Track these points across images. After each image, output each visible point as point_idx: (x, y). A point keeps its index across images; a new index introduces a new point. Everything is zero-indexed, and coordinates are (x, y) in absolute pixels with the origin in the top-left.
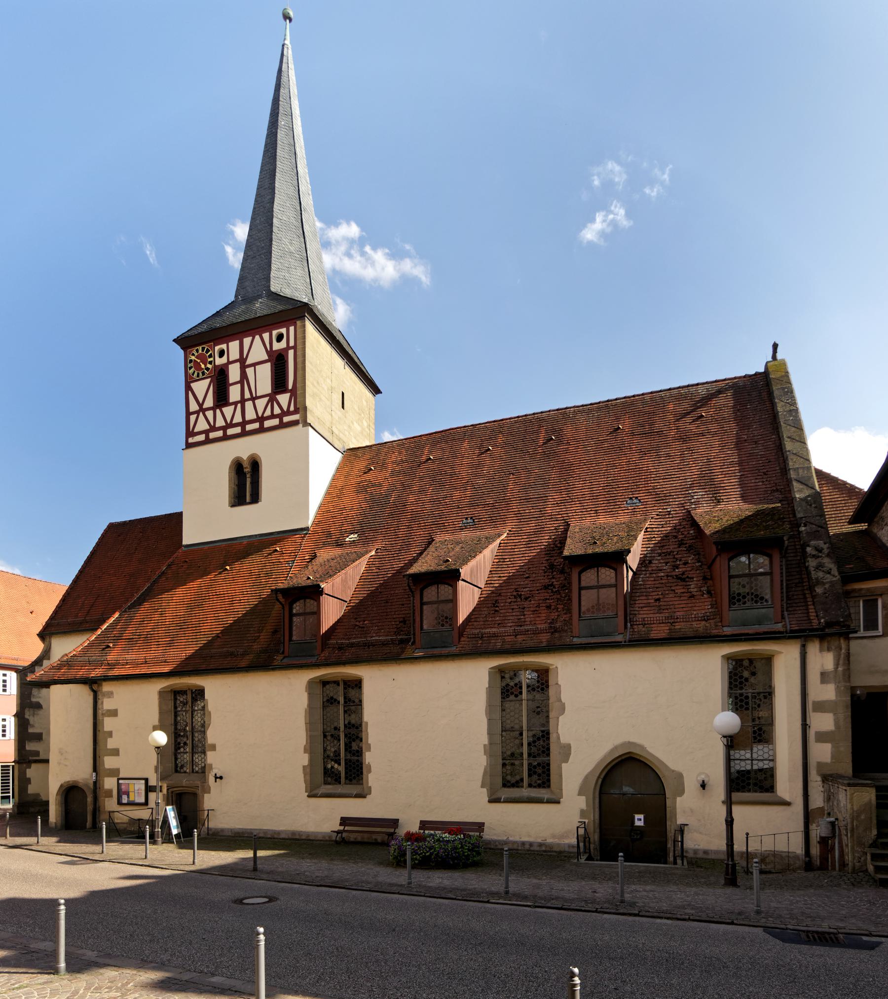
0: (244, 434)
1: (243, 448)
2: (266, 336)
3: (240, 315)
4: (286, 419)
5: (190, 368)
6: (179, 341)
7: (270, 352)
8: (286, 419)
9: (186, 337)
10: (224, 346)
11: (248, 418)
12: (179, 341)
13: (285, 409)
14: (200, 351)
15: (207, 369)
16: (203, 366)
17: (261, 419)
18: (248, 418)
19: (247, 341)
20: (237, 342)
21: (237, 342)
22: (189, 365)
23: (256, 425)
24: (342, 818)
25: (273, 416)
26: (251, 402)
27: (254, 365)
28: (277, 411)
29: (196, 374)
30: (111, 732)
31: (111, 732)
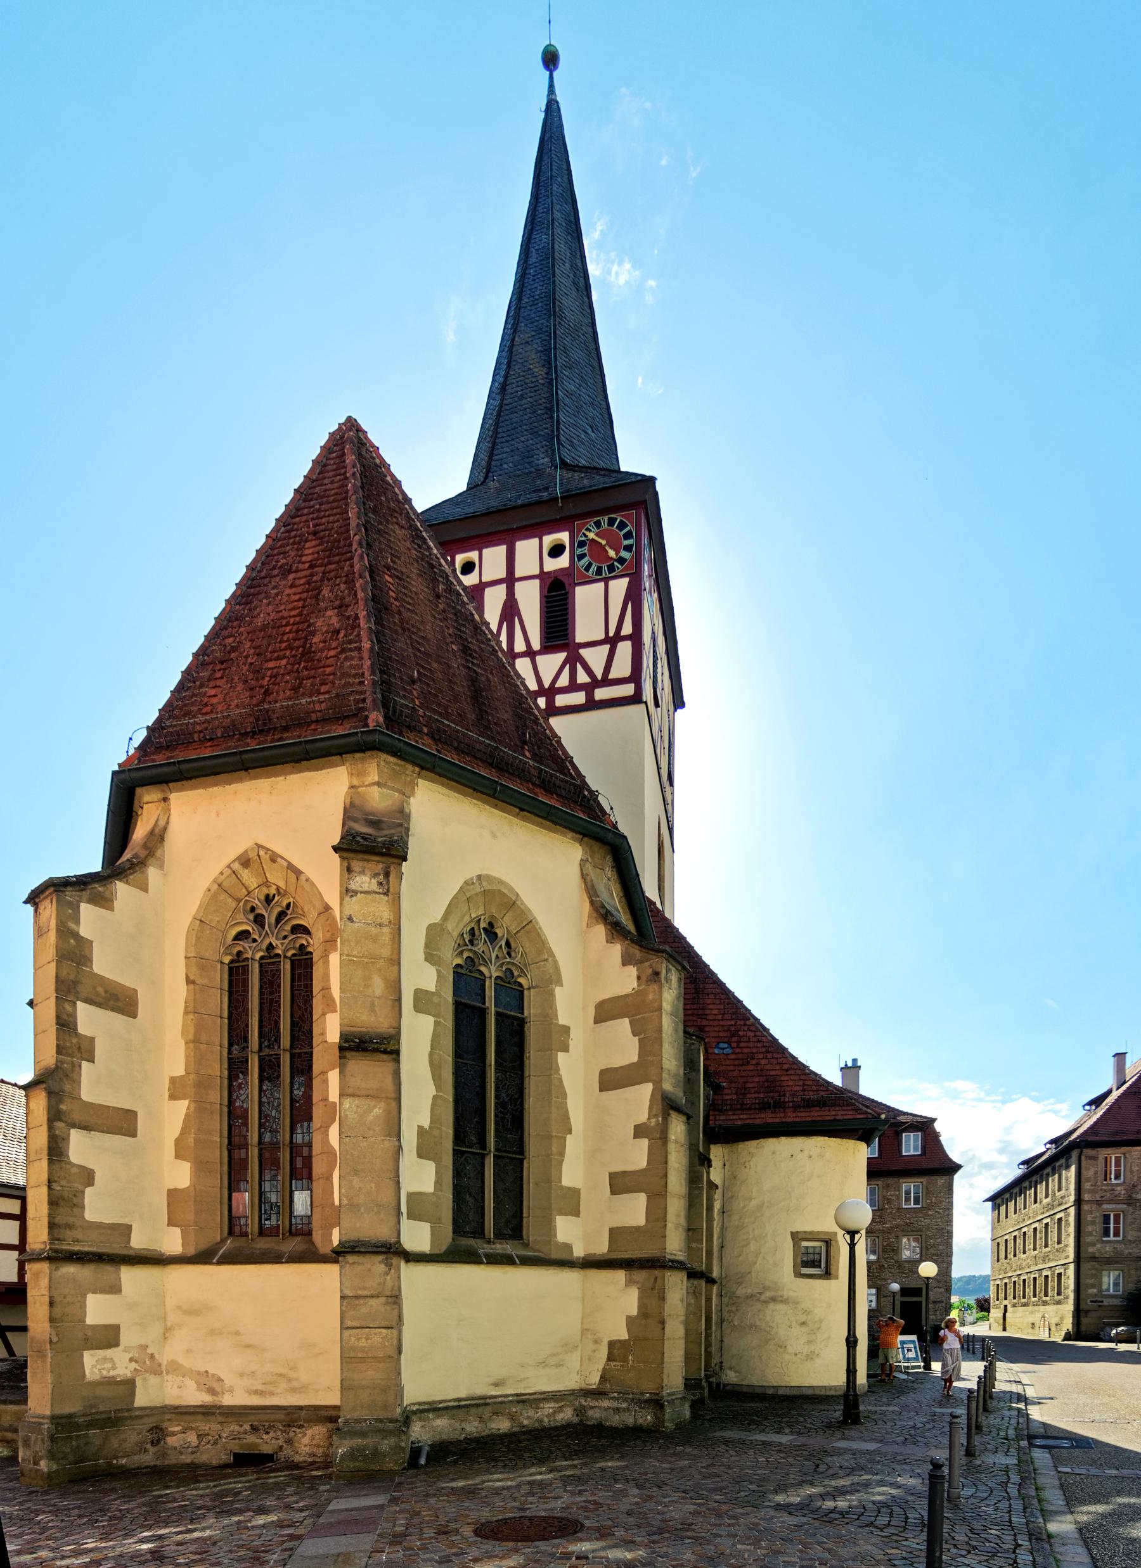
4: (600, 694)
5: (581, 557)
8: (600, 694)
10: (473, 555)
13: (599, 675)
14: (605, 525)
15: (621, 560)
16: (612, 553)
19: (521, 546)
20: (502, 549)
21: (502, 549)
24: (613, 1176)
25: (573, 687)
28: (582, 677)
29: (594, 568)
30: (637, 1135)
31: (637, 1135)
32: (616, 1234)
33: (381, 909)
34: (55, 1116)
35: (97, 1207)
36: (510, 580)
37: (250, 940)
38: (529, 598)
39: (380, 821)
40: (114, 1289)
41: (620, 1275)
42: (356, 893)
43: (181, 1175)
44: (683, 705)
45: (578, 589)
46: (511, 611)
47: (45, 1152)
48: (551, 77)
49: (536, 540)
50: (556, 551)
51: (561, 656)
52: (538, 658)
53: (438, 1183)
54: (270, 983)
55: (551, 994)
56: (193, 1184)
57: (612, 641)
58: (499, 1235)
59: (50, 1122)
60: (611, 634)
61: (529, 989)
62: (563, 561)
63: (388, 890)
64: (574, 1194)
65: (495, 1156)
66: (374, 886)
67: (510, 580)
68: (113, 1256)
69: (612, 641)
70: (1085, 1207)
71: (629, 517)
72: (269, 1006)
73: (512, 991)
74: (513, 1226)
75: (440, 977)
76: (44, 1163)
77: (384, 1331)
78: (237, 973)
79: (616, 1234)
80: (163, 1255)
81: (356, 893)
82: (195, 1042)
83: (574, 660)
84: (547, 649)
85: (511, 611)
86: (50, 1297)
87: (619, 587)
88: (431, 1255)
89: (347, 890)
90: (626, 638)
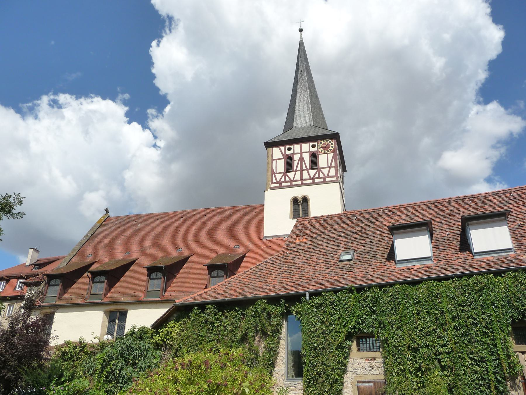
0: (292, 186)
1: (299, 192)
2: (282, 148)
4: (327, 179)
6: (265, 143)
10: (292, 147)
17: (313, 179)
23: (311, 181)
25: (319, 178)
38: (307, 157)
48: (301, 35)
50: (314, 146)
57: (329, 167)
62: (315, 149)
67: (301, 153)
69: (329, 167)
70: (219, 275)
83: (319, 170)
85: (302, 159)
90: (333, 167)
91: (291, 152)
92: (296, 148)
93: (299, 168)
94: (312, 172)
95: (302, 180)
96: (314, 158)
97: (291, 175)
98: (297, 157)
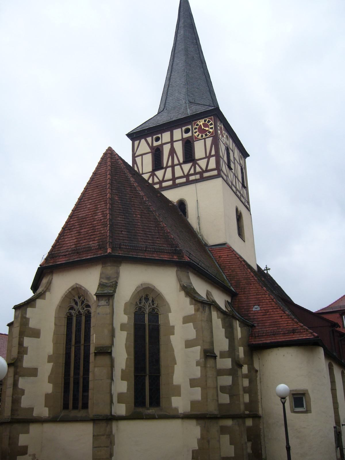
2: (149, 139)
3: (165, 119)
4: (206, 175)
5: (195, 133)
6: (129, 135)
7: (151, 147)
8: (206, 175)
9: (129, 134)
10: (160, 136)
11: (177, 175)
12: (129, 135)
13: (204, 169)
18: (177, 175)
22: (194, 131)
23: (184, 180)
25: (195, 173)
26: (179, 166)
27: (142, 155)
29: (200, 135)
32: (193, 403)
33: (108, 310)
34: (15, 373)
35: (25, 402)
36: (172, 142)
37: (36, 459)
38: (179, 147)
39: (110, 277)
40: (27, 432)
41: (193, 422)
42: (100, 306)
43: (49, 388)
44: (248, 155)
45: (195, 142)
46: (172, 152)
47: (12, 386)
49: (180, 129)
50: (187, 131)
51: (190, 165)
52: (183, 166)
53: (128, 389)
54: (79, 323)
55: (168, 316)
56: (53, 392)
57: (208, 157)
58: (151, 404)
59: (14, 376)
60: (208, 155)
61: (160, 315)
63: (109, 304)
64: (178, 387)
65: (149, 376)
66: (105, 303)
67: (172, 142)
68: (28, 420)
69: (208, 157)
71: (211, 119)
72: (78, 330)
73: (154, 316)
74: (156, 401)
75: (129, 318)
76: (12, 389)
77: (106, 448)
78: (69, 319)
79: (193, 403)
80: (42, 418)
81: (100, 306)
82: (56, 343)
84: (185, 162)
85: (172, 152)
86: (10, 436)
87: (209, 141)
88: (126, 416)
89: (98, 306)
90: (213, 156)
91: (159, 143)
92: (166, 137)
93: (170, 163)
94: (187, 167)
95: (174, 179)
96: (188, 146)
97: (160, 174)
98: (166, 149)
